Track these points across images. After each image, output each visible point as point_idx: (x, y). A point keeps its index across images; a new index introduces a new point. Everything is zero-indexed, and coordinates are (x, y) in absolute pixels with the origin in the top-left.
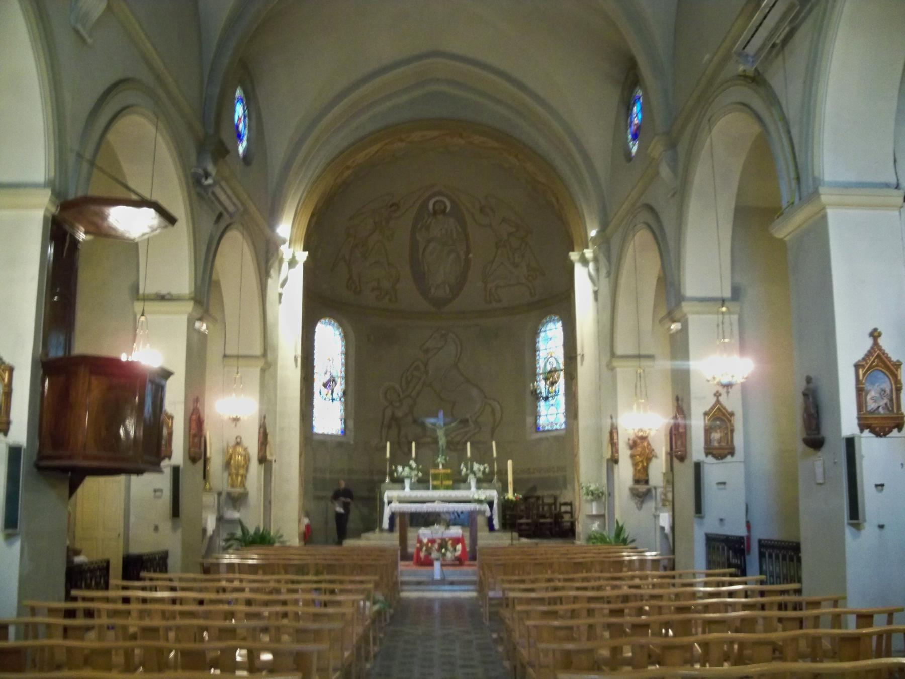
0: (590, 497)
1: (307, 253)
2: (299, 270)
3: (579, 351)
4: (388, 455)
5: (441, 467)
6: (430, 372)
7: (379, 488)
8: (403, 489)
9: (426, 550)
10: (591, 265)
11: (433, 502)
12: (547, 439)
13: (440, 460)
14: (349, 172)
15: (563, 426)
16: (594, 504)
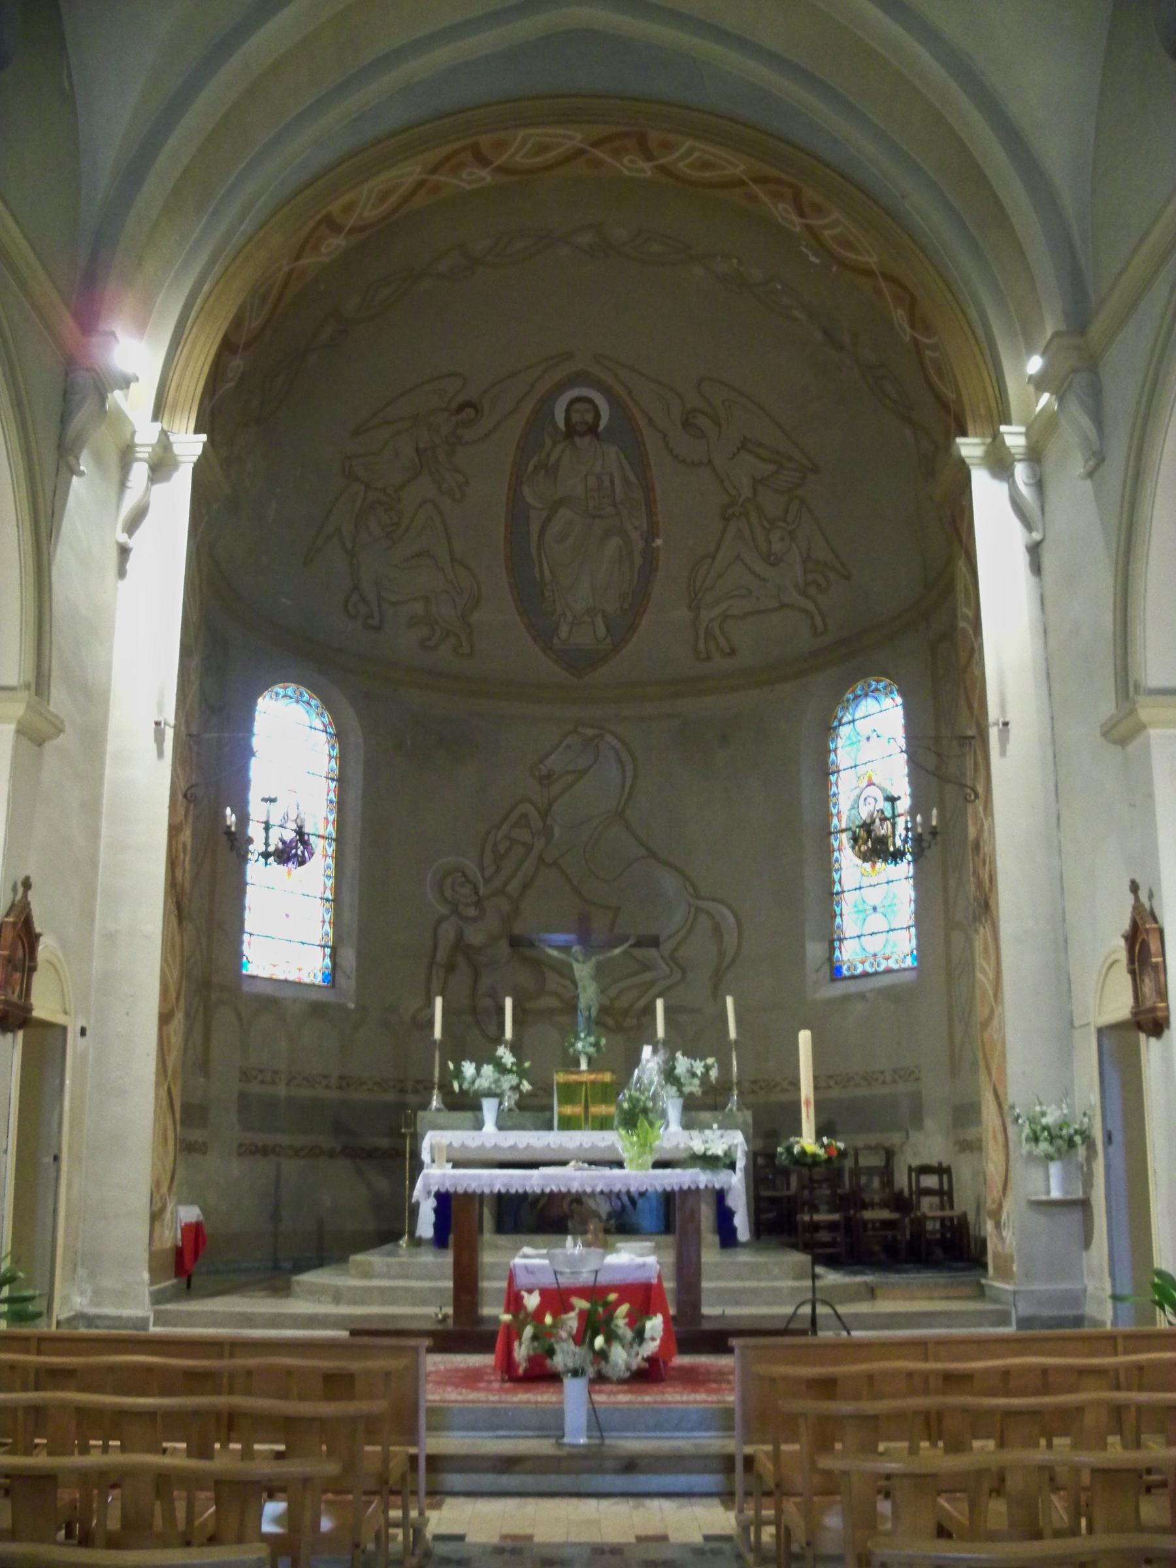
0: (1044, 1146)
1: (204, 437)
2: (181, 485)
3: (993, 713)
4: (438, 1033)
5: (584, 1066)
6: (557, 831)
7: (412, 1122)
8: (479, 1125)
9: (535, 1338)
10: (1020, 471)
11: (563, 1163)
12: (862, 996)
13: (582, 1045)
14: (335, 244)
15: (909, 962)
16: (1055, 1169)
